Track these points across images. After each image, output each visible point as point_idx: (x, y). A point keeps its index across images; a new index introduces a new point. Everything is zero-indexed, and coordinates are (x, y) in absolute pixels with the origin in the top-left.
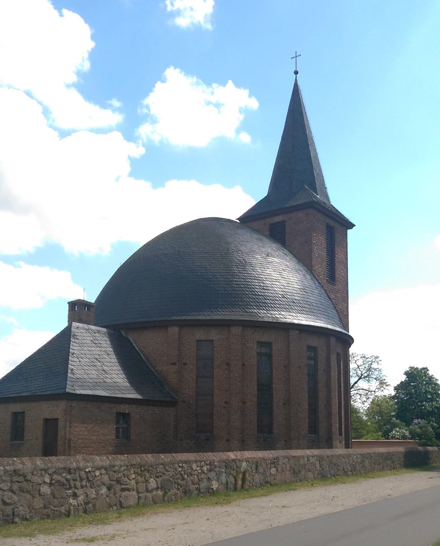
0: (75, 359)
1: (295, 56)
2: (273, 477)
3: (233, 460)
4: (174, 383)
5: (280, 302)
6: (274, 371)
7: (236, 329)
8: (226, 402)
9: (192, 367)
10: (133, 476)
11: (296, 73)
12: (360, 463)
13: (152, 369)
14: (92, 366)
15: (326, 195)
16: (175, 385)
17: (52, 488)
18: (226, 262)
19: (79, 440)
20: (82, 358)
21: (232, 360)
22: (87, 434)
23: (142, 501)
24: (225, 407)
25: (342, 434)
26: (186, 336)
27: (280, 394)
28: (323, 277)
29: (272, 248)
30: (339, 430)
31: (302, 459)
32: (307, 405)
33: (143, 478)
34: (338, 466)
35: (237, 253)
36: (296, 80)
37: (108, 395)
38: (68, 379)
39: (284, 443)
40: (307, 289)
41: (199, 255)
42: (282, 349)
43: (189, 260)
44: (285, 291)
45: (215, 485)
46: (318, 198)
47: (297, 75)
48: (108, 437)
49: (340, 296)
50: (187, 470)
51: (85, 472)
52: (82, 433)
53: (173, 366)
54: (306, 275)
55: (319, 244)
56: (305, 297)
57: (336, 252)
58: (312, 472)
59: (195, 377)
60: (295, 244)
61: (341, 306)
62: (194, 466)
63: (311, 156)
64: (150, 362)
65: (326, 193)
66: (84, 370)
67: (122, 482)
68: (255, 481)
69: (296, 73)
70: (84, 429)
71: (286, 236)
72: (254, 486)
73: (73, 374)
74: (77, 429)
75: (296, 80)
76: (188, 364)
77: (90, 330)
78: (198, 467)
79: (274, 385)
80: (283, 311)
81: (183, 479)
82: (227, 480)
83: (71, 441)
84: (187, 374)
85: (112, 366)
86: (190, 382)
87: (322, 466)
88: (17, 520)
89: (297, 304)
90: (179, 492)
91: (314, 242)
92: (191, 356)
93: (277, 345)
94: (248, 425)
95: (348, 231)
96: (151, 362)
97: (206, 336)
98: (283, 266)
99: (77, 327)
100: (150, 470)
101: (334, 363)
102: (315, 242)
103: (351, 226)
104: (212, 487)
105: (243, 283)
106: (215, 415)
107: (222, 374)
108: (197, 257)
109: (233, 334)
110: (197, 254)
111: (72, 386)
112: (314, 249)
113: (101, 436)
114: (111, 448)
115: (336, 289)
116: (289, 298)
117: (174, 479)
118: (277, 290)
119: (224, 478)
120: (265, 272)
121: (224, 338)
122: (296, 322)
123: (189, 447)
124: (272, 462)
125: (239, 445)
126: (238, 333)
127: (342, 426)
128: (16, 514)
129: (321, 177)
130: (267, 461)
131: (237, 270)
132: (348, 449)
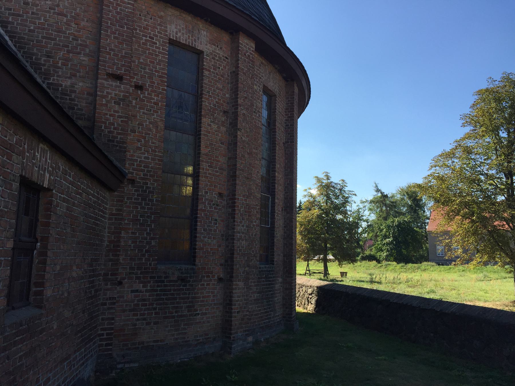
4: (115, 129)
9: (155, 98)
24: (217, 205)
26: (145, 20)
64: (31, 58)
76: (148, 90)
84: (144, 113)
86: (149, 134)
97: (189, 36)
106: (201, 222)
123: (138, 301)
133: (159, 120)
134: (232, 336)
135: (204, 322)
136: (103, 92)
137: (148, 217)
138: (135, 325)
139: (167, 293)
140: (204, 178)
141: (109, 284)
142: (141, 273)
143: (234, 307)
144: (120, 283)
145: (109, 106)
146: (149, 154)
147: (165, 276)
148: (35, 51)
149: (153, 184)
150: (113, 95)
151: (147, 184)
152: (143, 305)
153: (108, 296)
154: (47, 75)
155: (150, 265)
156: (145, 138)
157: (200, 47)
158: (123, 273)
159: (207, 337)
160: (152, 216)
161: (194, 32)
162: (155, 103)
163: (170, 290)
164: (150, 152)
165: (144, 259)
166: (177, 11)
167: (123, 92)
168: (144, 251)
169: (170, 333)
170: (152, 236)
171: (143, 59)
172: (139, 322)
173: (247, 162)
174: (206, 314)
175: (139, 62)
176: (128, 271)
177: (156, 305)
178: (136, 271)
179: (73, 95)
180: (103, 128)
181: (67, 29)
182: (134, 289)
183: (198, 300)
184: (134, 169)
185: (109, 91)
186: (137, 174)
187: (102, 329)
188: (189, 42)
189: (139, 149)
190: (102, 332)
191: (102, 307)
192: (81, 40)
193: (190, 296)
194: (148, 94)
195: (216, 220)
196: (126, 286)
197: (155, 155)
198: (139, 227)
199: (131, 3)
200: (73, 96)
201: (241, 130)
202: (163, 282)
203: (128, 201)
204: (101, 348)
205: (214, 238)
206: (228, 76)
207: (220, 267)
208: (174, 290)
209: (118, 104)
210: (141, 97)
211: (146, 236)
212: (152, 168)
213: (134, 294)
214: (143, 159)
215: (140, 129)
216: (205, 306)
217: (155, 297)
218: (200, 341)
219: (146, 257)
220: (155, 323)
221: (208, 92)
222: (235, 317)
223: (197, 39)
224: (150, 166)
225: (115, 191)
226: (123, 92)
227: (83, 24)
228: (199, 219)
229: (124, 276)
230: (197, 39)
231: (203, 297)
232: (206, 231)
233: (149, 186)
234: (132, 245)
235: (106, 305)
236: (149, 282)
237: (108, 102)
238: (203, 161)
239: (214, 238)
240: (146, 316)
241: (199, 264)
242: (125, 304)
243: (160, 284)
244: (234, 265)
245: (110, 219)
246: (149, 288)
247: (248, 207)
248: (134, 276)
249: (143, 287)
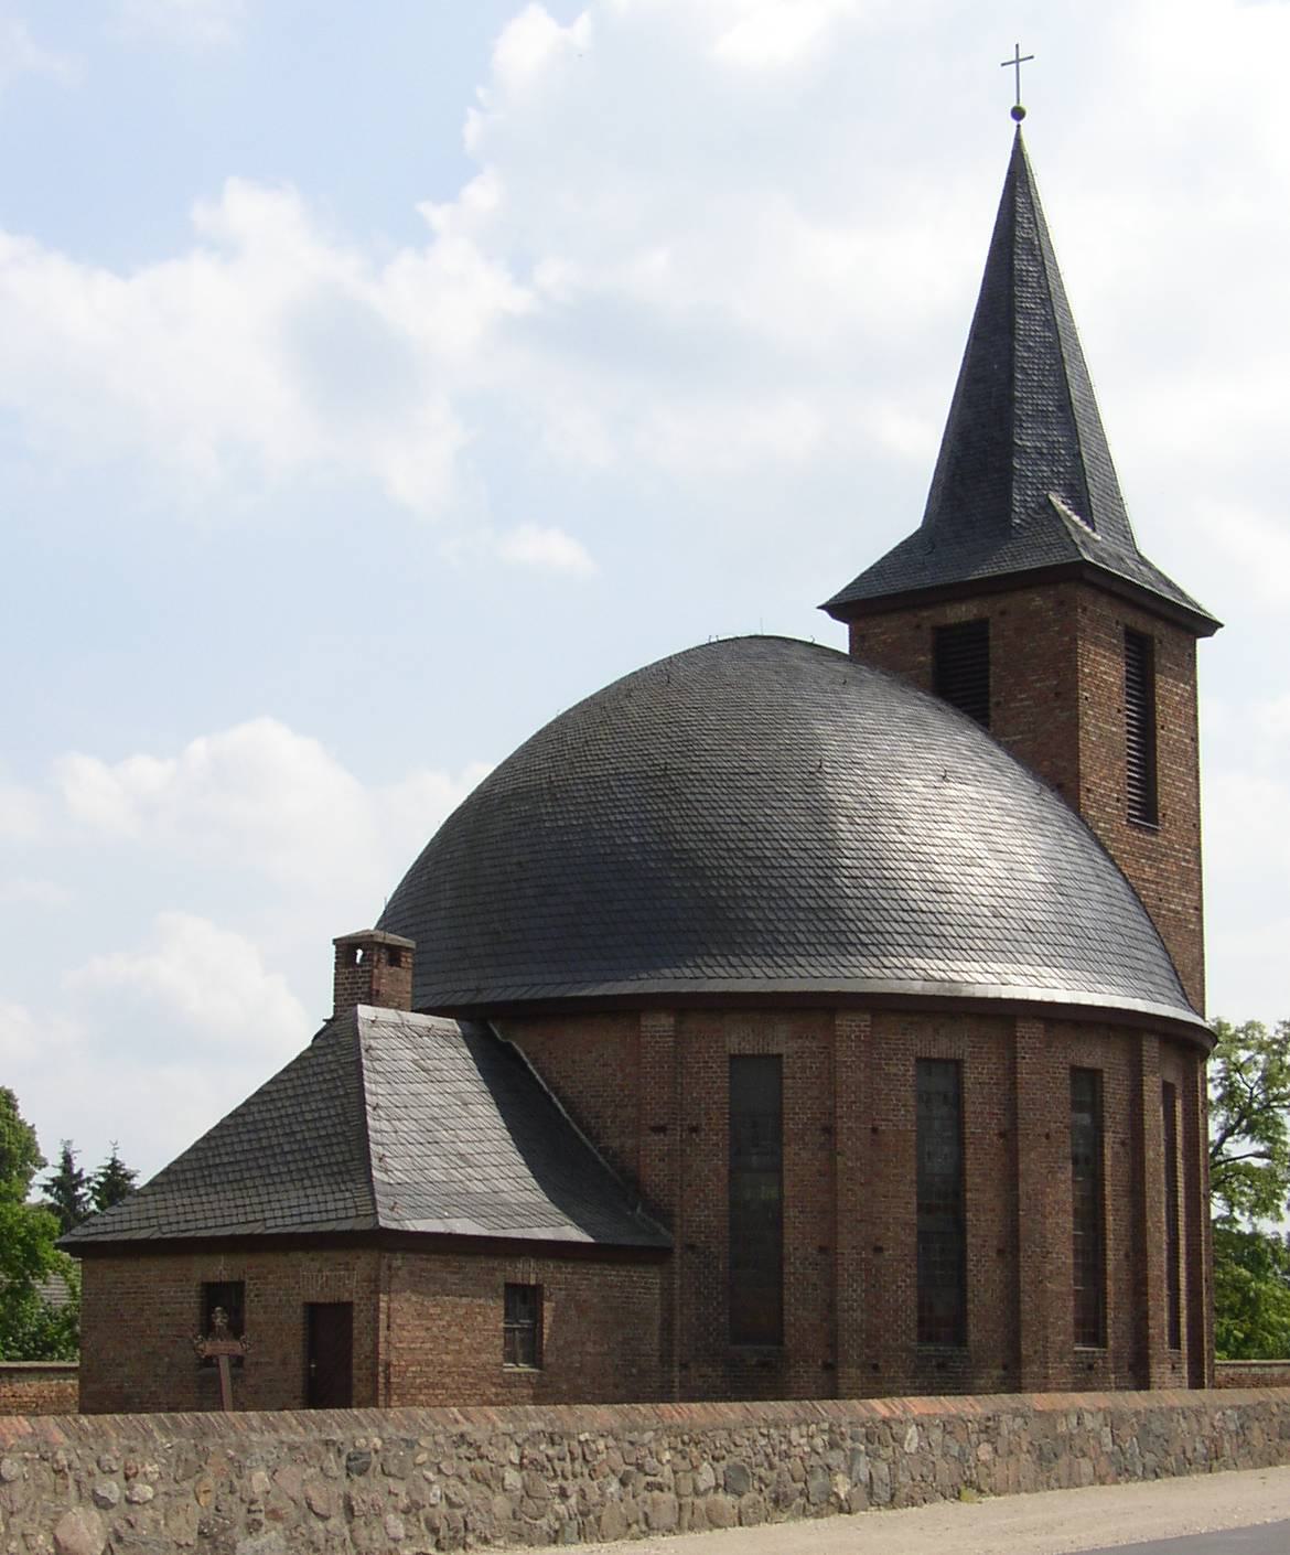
0: (385, 1125)
1: (1014, 58)
2: (986, 1470)
3: (885, 1422)
5: (986, 930)
6: (970, 1151)
7: (852, 1021)
9: (715, 1138)
10: (667, 1456)
11: (1018, 114)
12: (1233, 1435)
14: (429, 1143)
15: (1125, 526)
16: (665, 1195)
17: (524, 1473)
18: (816, 804)
19: (411, 1365)
20: (399, 1120)
21: (841, 1117)
22: (431, 1349)
23: (687, 1516)
25: (1180, 1344)
27: (987, 1220)
28: (1117, 808)
29: (957, 749)
30: (1170, 1330)
31: (1064, 1420)
32: (1071, 1254)
33: (688, 1460)
34: (1167, 1441)
35: (850, 774)
36: (1018, 141)
37: (485, 1232)
38: (377, 1186)
39: (1002, 1372)
40: (1067, 882)
41: (731, 780)
42: (995, 1081)
43: (700, 797)
44: (1002, 894)
45: (843, 1487)
46: (1096, 541)
47: (1021, 123)
48: (484, 1357)
49: (1174, 869)
50: (778, 1443)
51: (580, 1442)
52: (419, 1345)
53: (656, 1138)
54: (1063, 836)
55: (1103, 701)
56: (1064, 911)
57: (1159, 720)
58: (1091, 1458)
59: (724, 1171)
60: (1022, 700)
61: (1178, 904)
62: (794, 1434)
63: (1070, 396)
65: (1123, 519)
66: (411, 1157)
67: (647, 1469)
68: (938, 1478)
69: (1018, 114)
70: (423, 1334)
71: (991, 672)
72: (937, 1491)
73: (386, 1171)
74: (405, 1333)
75: (1018, 141)
77: (407, 1029)
78: (802, 1436)
79: (969, 1195)
80: (994, 959)
81: (772, 1467)
82: (870, 1474)
83: (392, 1369)
85: (481, 1141)
87: (1118, 1441)
88: (470, 1539)
89: (1038, 935)
90: (761, 1500)
91: (1085, 694)
93: (977, 1068)
94: (891, 1319)
95: (1200, 642)
98: (992, 811)
99: (373, 1022)
100: (700, 1442)
101: (1154, 1119)
102: (1088, 695)
103: (1209, 626)
104: (836, 1490)
105: (870, 872)
106: (789, 1289)
107: (809, 1160)
108: (767, 840)
109: (842, 1036)
110: (724, 777)
111: (392, 1209)
112: (1086, 719)
113: (466, 1352)
114: (494, 1390)
115: (1159, 845)
116: (1014, 916)
117: (750, 1465)
118: (975, 892)
119: (863, 1468)
120: (938, 833)
121: (814, 1049)
122: (1036, 995)
124: (983, 1428)
127: (1179, 1317)
128: (470, 1526)
129: (1105, 467)
130: (969, 1424)
131: (850, 832)
132: (1198, 1391)
150: (657, 1152)
157: (774, 1050)
175: (692, 1098)
194: (706, 1135)
195: (815, 1284)
199: (558, 1110)
238: (788, 1206)
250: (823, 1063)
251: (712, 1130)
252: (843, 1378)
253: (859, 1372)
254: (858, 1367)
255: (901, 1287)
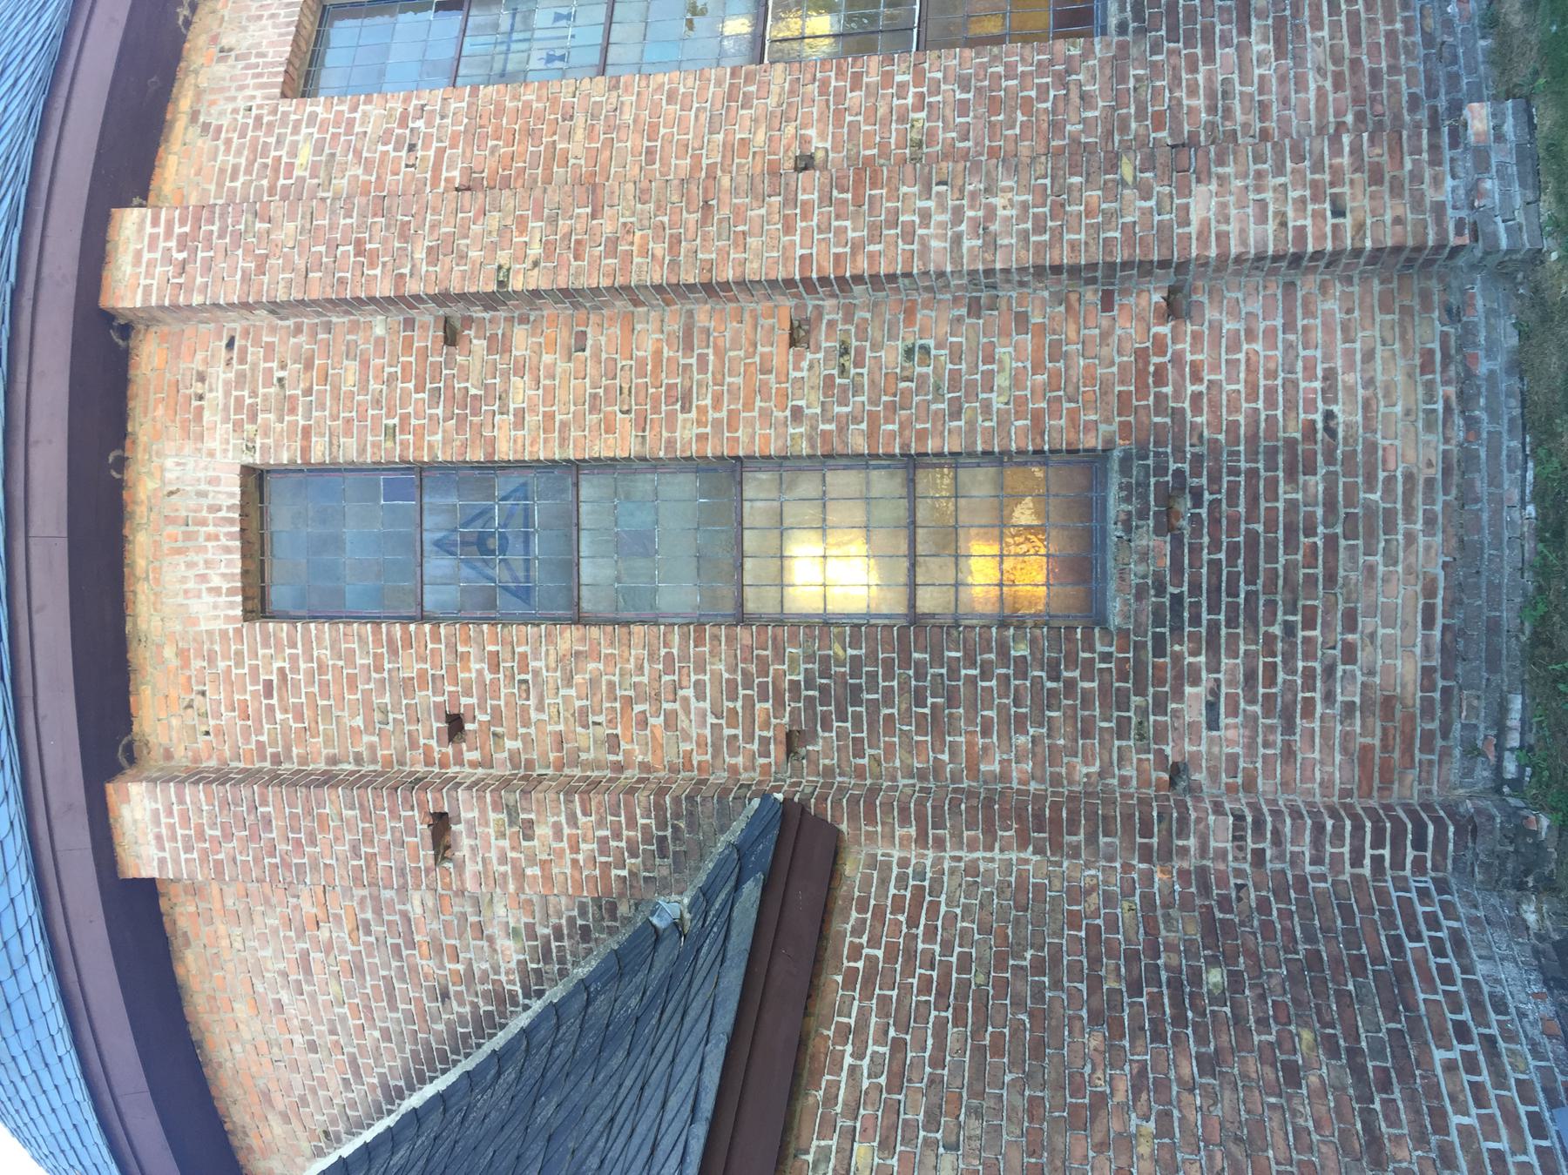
8: (793, 342)
9: (475, 666)
13: (523, 1020)
16: (632, 822)
24: (845, 351)
59: (568, 638)
64: (466, 1036)
84: (540, 708)
86: (611, 685)
92: (379, 669)
94: (1020, 118)
96: (464, 1024)
97: (209, 538)
106: (922, 435)
123: (1252, 701)
125: (1229, 170)
126: (173, 244)
133: (552, 651)
134: (1453, 240)
135: (1369, 383)
136: (504, 875)
137: (920, 676)
138: (1349, 708)
139: (1224, 578)
140: (740, 434)
141: (1180, 843)
142: (1142, 691)
143: (1310, 240)
144: (1177, 771)
145: (545, 857)
146: (684, 683)
147: (1152, 592)
148: (441, 1027)
149: (794, 661)
150: (506, 843)
151: (795, 685)
152: (1271, 681)
153: (1229, 845)
154: (503, 999)
155: (1106, 657)
156: (628, 702)
157: (230, 490)
158: (1140, 760)
159: (1438, 356)
160: (916, 663)
161: (184, 514)
162: (495, 667)
163: (1215, 565)
164: (676, 678)
165: (1087, 685)
166: (134, 593)
167: (483, 811)
168: (1054, 685)
169: (1401, 555)
170: (993, 656)
171: (352, 716)
172: (1339, 690)
173: (633, 214)
174: (1329, 375)
176: (1131, 743)
177: (1272, 623)
178: (1131, 714)
179: (542, 931)
180: (625, 873)
181: (343, 950)
182: (1203, 719)
183: (1263, 425)
184: (750, 738)
185: (493, 855)
186: (766, 725)
187: (1357, 861)
188: (229, 535)
189: (671, 721)
190: (1367, 861)
191: (1269, 865)
192: (363, 910)
193: (1243, 465)
194: (469, 694)
195: (909, 353)
196: (1188, 748)
197: (684, 657)
198: (961, 710)
200: (546, 931)
201: (500, 267)
202: (1177, 600)
203: (868, 751)
204: (1429, 865)
205: (989, 359)
206: (298, 330)
207: (1115, 312)
208: (1215, 546)
209: (531, 827)
210: (486, 718)
211: (994, 683)
212: (732, 669)
213: (1222, 716)
214: (707, 705)
215: (601, 719)
216: (1295, 384)
217: (1240, 631)
218: (1453, 398)
219: (1077, 674)
220: (1350, 623)
221: (390, 432)
222: (1360, 227)
223: (205, 502)
224: (726, 675)
225: (839, 832)
226: (483, 811)
227: (309, 908)
228: (909, 446)
229: (1151, 756)
230: (205, 502)
231: (1252, 395)
232: (961, 408)
233: (801, 678)
234: (1031, 731)
235: (1263, 850)
236: (1177, 658)
237: (532, 860)
238: (671, 443)
239: (989, 359)
240: (1317, 665)
241: (1103, 427)
242: (1261, 751)
243: (1186, 614)
244: (1108, 259)
245: (939, 844)
246: (1202, 659)
247: (835, 193)
248: (1152, 718)
249: (1196, 682)
250: (270, 348)
251: (452, 669)
252: (1222, 237)
253: (1199, 190)
254: (1185, 191)
255: (921, 96)
